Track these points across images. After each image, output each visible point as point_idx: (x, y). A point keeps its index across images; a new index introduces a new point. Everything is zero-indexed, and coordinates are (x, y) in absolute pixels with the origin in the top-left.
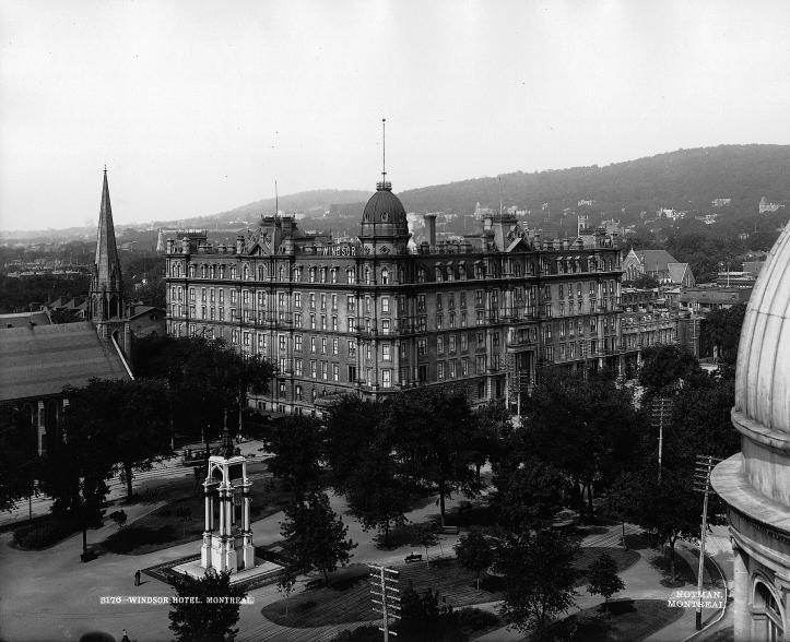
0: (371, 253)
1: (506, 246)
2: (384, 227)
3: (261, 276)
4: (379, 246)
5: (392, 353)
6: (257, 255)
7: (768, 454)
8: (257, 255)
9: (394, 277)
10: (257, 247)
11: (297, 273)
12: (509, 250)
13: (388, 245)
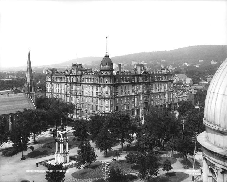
0: (103, 74)
1: (140, 73)
2: (107, 67)
3: (72, 81)
4: (105, 72)
5: (109, 102)
6: (71, 75)
7: (213, 132)
8: (71, 75)
9: (109, 81)
10: (71, 73)
11: (82, 80)
12: (141, 74)
13: (108, 72)
